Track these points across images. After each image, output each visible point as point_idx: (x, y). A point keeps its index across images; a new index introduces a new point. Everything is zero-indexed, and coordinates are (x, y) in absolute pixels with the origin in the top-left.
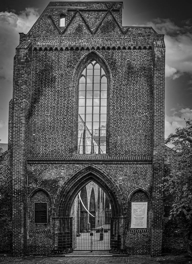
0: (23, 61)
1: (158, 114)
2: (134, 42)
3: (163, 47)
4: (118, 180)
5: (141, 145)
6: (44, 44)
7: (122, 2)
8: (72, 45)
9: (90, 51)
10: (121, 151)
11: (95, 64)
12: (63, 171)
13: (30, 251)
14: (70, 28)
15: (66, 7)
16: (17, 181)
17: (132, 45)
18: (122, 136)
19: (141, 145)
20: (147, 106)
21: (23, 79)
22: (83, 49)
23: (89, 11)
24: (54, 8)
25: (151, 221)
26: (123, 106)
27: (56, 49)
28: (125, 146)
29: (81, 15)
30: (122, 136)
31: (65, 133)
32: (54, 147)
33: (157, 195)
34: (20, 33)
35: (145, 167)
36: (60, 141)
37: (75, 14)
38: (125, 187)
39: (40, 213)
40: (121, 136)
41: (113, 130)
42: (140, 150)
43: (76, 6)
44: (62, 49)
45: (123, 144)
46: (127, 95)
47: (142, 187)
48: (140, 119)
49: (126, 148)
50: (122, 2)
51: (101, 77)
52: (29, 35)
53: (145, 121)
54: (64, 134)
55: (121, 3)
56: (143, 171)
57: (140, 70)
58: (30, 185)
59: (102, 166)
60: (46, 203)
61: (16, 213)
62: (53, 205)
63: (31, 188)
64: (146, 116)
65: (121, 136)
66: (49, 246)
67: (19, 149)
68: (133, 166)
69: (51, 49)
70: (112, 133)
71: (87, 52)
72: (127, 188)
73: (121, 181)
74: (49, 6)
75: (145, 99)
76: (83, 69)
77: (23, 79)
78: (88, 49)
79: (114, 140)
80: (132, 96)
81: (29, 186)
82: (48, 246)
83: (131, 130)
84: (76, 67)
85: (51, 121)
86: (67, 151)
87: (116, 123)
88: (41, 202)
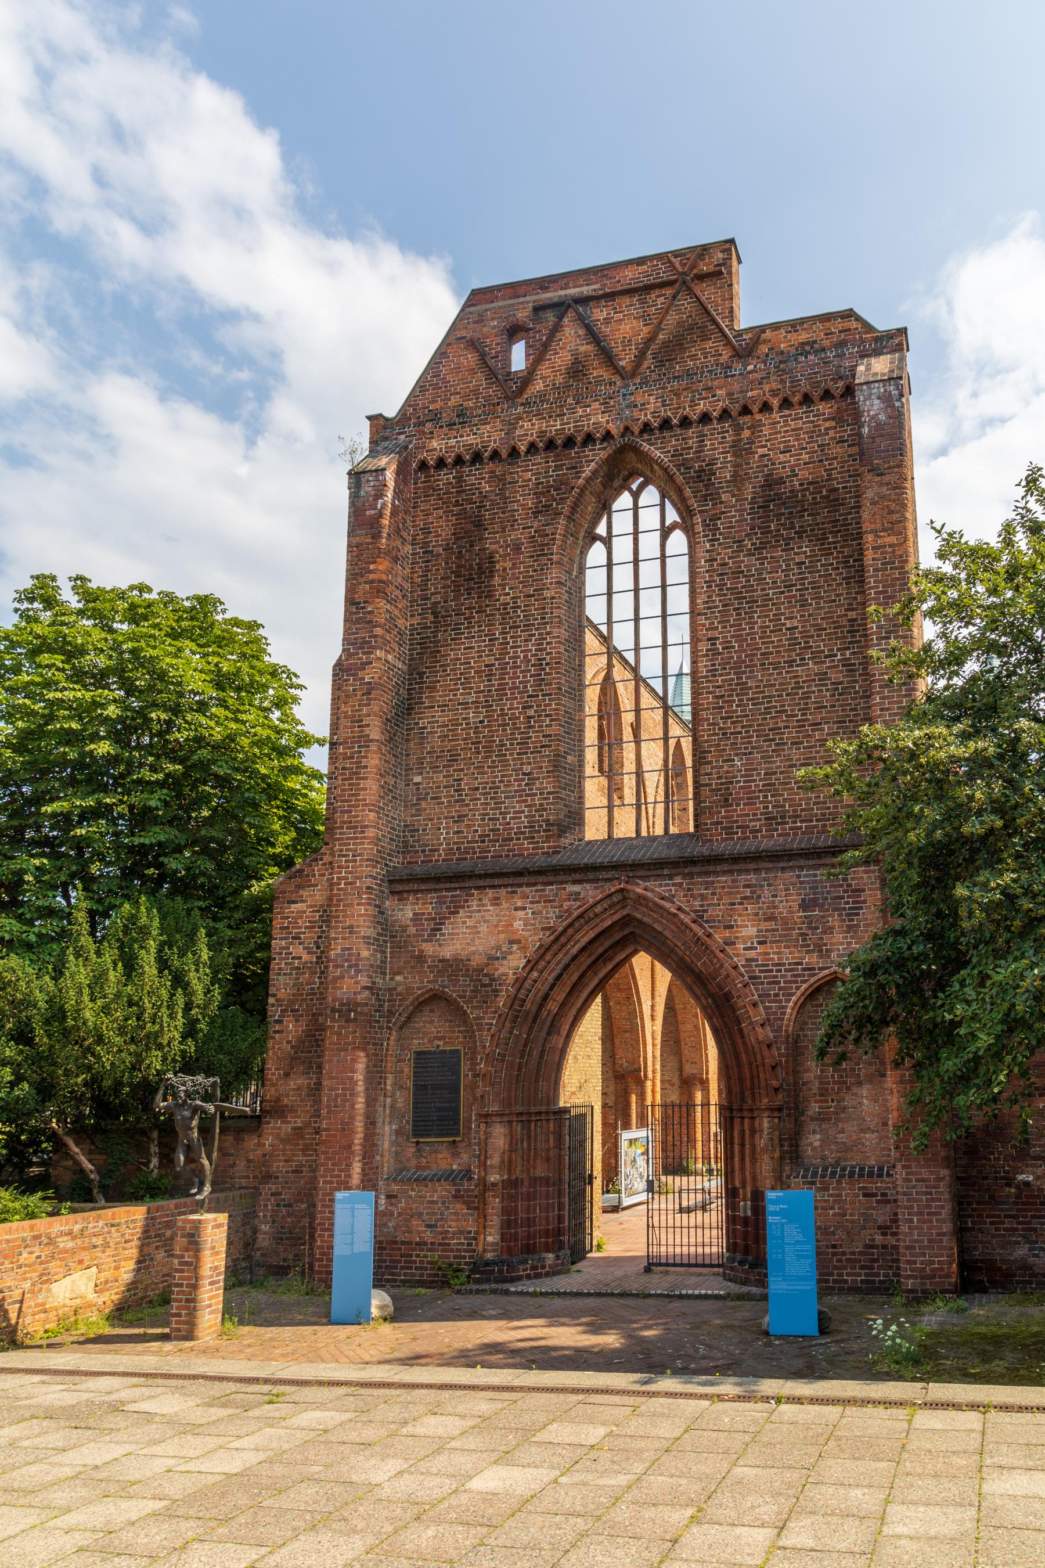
0: (373, 512)
2: (782, 381)
4: (737, 938)
8: (551, 431)
9: (619, 442)
10: (748, 815)
12: (521, 913)
14: (544, 370)
15: (528, 298)
16: (343, 966)
18: (750, 753)
20: (850, 620)
21: (371, 576)
22: (589, 439)
23: (610, 296)
24: (487, 310)
26: (748, 634)
28: (766, 797)
30: (750, 753)
31: (529, 763)
34: (369, 418)
36: (513, 797)
37: (560, 318)
38: (772, 971)
39: (434, 1094)
40: (745, 754)
42: (829, 808)
43: (561, 289)
44: (514, 452)
45: (757, 786)
48: (823, 676)
49: (771, 802)
51: (665, 532)
52: (403, 417)
53: (841, 683)
54: (527, 769)
57: (809, 483)
58: (398, 978)
59: (674, 885)
60: (458, 1051)
62: (481, 1059)
63: (400, 989)
65: (745, 754)
66: (463, 1244)
67: (357, 838)
68: (799, 876)
70: (709, 746)
71: (604, 449)
72: (780, 971)
73: (752, 943)
74: (471, 306)
75: (838, 595)
77: (371, 576)
78: (608, 436)
79: (718, 773)
80: (782, 592)
82: (459, 1244)
84: (566, 510)
85: (481, 722)
87: (722, 708)
88: (438, 1046)
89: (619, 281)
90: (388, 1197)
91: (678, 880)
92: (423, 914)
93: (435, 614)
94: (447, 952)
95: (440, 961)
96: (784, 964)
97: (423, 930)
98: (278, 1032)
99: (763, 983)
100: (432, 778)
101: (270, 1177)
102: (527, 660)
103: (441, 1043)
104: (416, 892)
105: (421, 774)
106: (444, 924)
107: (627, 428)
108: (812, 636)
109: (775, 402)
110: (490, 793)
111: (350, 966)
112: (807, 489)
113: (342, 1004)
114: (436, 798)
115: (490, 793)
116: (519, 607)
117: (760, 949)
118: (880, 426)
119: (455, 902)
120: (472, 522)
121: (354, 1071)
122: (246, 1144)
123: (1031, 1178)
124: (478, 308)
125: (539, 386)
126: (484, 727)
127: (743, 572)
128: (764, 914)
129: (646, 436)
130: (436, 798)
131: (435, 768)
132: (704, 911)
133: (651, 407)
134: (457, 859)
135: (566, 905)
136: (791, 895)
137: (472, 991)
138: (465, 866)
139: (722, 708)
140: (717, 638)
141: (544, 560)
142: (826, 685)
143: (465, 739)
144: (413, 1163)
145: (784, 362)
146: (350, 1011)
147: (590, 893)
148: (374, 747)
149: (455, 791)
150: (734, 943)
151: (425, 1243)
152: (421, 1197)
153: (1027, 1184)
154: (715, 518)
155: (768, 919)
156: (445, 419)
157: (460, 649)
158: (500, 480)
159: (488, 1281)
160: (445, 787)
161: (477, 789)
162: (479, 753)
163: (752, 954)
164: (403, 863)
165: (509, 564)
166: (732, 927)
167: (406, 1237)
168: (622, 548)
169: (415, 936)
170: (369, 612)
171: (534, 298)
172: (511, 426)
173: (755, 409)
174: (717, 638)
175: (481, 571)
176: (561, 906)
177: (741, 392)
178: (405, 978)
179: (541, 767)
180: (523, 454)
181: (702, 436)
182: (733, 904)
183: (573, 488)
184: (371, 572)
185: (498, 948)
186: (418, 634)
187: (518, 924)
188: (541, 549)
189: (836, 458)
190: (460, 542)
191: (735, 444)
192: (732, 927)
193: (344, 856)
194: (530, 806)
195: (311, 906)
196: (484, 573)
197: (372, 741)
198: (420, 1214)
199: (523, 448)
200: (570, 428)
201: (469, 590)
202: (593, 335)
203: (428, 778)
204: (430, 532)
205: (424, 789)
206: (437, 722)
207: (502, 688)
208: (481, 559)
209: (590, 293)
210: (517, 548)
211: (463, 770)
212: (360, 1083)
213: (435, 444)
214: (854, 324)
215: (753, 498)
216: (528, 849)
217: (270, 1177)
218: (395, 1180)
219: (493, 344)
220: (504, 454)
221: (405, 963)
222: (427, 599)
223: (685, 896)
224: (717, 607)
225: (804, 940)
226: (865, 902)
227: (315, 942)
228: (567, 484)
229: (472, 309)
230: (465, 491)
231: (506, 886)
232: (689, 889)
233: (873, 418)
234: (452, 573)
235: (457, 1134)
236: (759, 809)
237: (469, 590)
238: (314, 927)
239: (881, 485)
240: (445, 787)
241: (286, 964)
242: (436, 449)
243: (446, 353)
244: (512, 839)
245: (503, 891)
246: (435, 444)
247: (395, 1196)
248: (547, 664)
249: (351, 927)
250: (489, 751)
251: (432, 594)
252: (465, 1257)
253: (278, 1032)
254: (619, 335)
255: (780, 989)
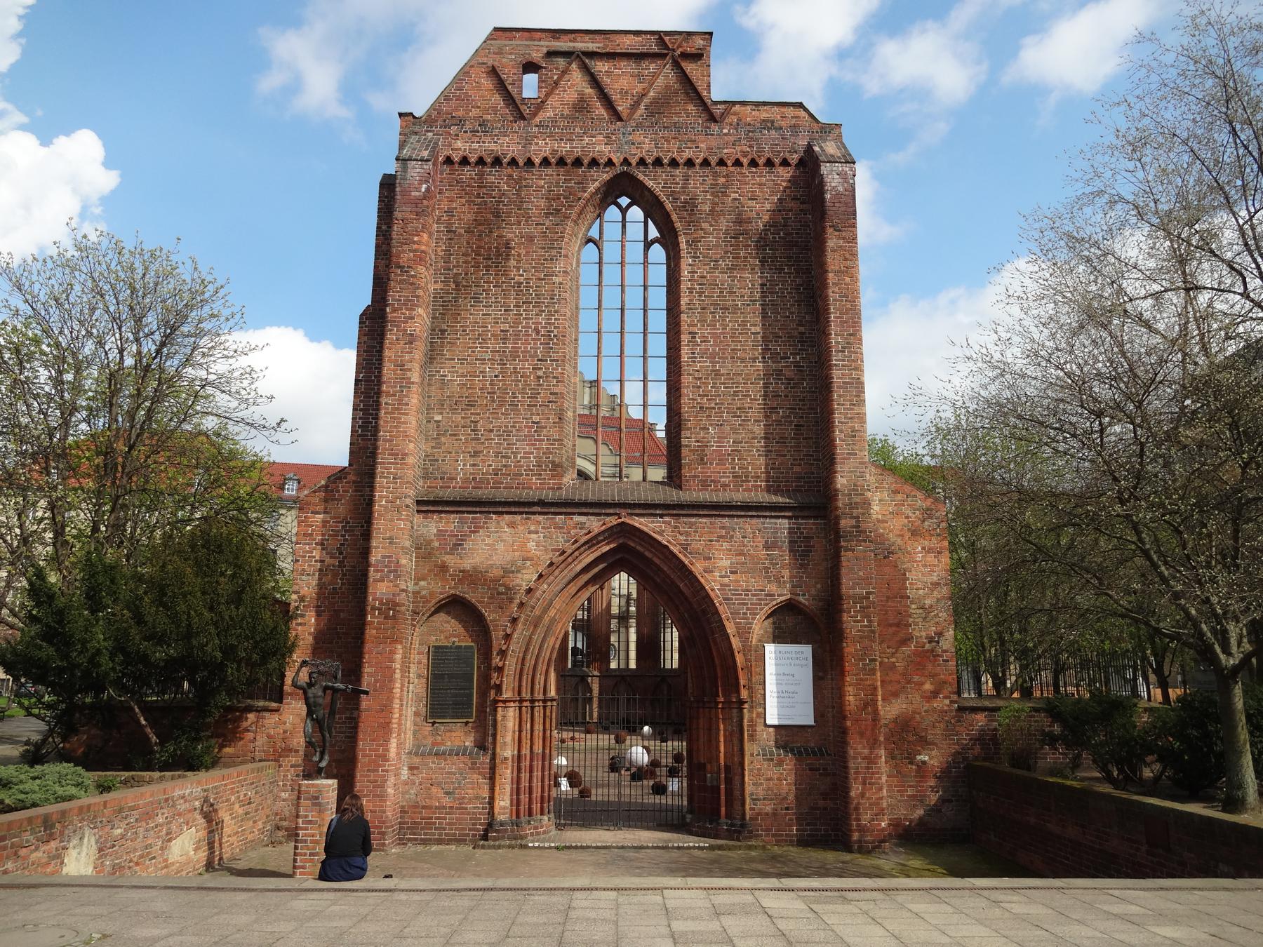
0: (417, 194)
1: (844, 360)
2: (751, 146)
3: (847, 162)
5: (785, 456)
6: (475, 145)
7: (711, 34)
9: (619, 169)
11: (629, 206)
12: (534, 536)
13: (408, 828)
14: (553, 101)
15: (542, 43)
16: (383, 571)
17: (745, 154)
19: (785, 456)
20: (800, 333)
21: (415, 246)
22: (594, 163)
24: (506, 46)
25: (834, 717)
26: (721, 333)
27: (513, 162)
29: (586, 69)
31: (538, 414)
32: (502, 457)
33: (854, 621)
34: (401, 115)
35: (804, 529)
36: (523, 440)
41: (694, 407)
44: (530, 162)
46: (734, 301)
47: (799, 595)
50: (711, 34)
51: (648, 245)
52: (429, 120)
53: (793, 379)
54: (537, 418)
55: (707, 36)
56: (797, 542)
58: (422, 583)
59: (663, 522)
61: (376, 681)
63: (424, 593)
64: (796, 365)
66: (478, 808)
67: (397, 463)
68: (764, 523)
69: (497, 161)
71: (607, 172)
76: (593, 222)
77: (415, 246)
78: (610, 163)
80: (749, 305)
81: (417, 588)
82: (474, 808)
83: (751, 408)
84: (574, 216)
85: (496, 376)
86: (546, 470)
87: (700, 387)
88: (454, 642)
89: (618, 45)
90: (411, 768)
91: (667, 519)
92: (447, 531)
93: (457, 284)
94: (467, 564)
95: (460, 571)
96: (750, 590)
97: (446, 544)
98: (300, 624)
99: (734, 604)
100: (451, 418)
101: (291, 751)
102: (538, 333)
103: (456, 639)
104: (441, 512)
105: (442, 413)
106: (465, 540)
107: (626, 160)
108: (771, 341)
109: (745, 161)
110: (503, 435)
111: (390, 572)
112: (769, 230)
113: (381, 603)
114: (455, 435)
115: (503, 435)
116: (532, 287)
117: (732, 577)
118: (838, 195)
119: (476, 523)
120: (491, 213)
121: (392, 661)
122: (266, 721)
123: (927, 758)
124: (498, 42)
125: (549, 113)
126: (500, 381)
127: (717, 285)
128: (736, 550)
129: (642, 168)
130: (455, 435)
131: (454, 411)
132: (688, 545)
133: (646, 147)
134: (473, 487)
135: (573, 532)
136: (757, 537)
137: (490, 598)
138: (484, 493)
139: (700, 387)
140: (696, 333)
141: (554, 252)
142: (781, 379)
143: (482, 389)
144: (429, 741)
145: (753, 132)
146: (390, 609)
147: (595, 524)
148: (414, 388)
149: (472, 430)
150: (712, 572)
151: (444, 808)
152: (440, 769)
153: (924, 763)
154: (696, 241)
155: (740, 554)
156: (468, 127)
157: (478, 315)
158: (517, 183)
159: (503, 838)
160: (463, 427)
161: (491, 431)
162: (493, 401)
163: (726, 580)
164: (423, 487)
165: (523, 252)
166: (710, 558)
167: (428, 802)
168: (611, 252)
169: (438, 549)
170: (412, 276)
171: (547, 43)
172: (527, 142)
173: (729, 163)
174: (696, 333)
175: (498, 254)
176: (569, 533)
177: (719, 148)
178: (429, 584)
179: (548, 419)
180: (537, 165)
181: (687, 178)
182: (712, 541)
183: (580, 199)
184: (414, 242)
185: (513, 563)
186: (441, 297)
187: (531, 545)
188: (553, 244)
189: (791, 210)
190: (480, 227)
191: (714, 186)
192: (710, 558)
193: (385, 477)
194: (538, 449)
195: (335, 518)
196: (501, 255)
197: (413, 383)
198: (439, 784)
199: (537, 161)
200: (578, 152)
201: (487, 268)
202: (595, 82)
203: (448, 418)
204: (453, 216)
205: (444, 426)
206: (457, 372)
207: (515, 350)
208: (499, 244)
209: (595, 50)
210: (531, 239)
211: (479, 414)
212: (398, 671)
213: (459, 144)
214: (803, 114)
215: (726, 230)
216: (536, 484)
217: (291, 751)
218: (416, 754)
219: (509, 74)
220: (521, 163)
221: (429, 571)
222: (449, 269)
223: (673, 531)
224: (697, 309)
225: (767, 572)
226: (813, 546)
227: (338, 549)
228: (575, 195)
229: (493, 42)
230: (485, 187)
231: (521, 513)
232: (676, 527)
233: (834, 187)
234: (473, 251)
235: (471, 717)
236: (727, 468)
237: (487, 268)
238: (337, 536)
239: (839, 238)
240: (463, 427)
241: (309, 566)
242: (460, 149)
243: (468, 73)
244: (522, 475)
245: (518, 517)
246: (459, 144)
247: (417, 768)
248: (555, 336)
249: (391, 538)
250: (503, 401)
251: (454, 266)
252: (480, 819)
253: (300, 624)
254: (616, 86)
255: (748, 609)
